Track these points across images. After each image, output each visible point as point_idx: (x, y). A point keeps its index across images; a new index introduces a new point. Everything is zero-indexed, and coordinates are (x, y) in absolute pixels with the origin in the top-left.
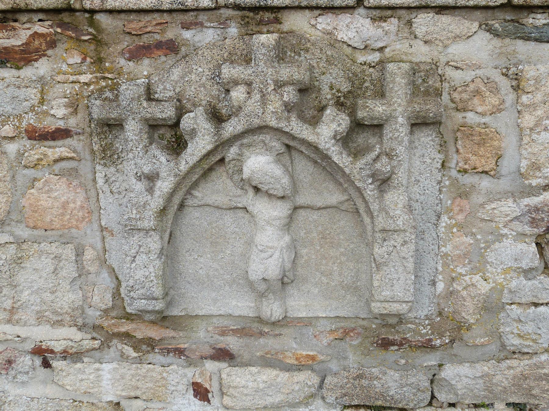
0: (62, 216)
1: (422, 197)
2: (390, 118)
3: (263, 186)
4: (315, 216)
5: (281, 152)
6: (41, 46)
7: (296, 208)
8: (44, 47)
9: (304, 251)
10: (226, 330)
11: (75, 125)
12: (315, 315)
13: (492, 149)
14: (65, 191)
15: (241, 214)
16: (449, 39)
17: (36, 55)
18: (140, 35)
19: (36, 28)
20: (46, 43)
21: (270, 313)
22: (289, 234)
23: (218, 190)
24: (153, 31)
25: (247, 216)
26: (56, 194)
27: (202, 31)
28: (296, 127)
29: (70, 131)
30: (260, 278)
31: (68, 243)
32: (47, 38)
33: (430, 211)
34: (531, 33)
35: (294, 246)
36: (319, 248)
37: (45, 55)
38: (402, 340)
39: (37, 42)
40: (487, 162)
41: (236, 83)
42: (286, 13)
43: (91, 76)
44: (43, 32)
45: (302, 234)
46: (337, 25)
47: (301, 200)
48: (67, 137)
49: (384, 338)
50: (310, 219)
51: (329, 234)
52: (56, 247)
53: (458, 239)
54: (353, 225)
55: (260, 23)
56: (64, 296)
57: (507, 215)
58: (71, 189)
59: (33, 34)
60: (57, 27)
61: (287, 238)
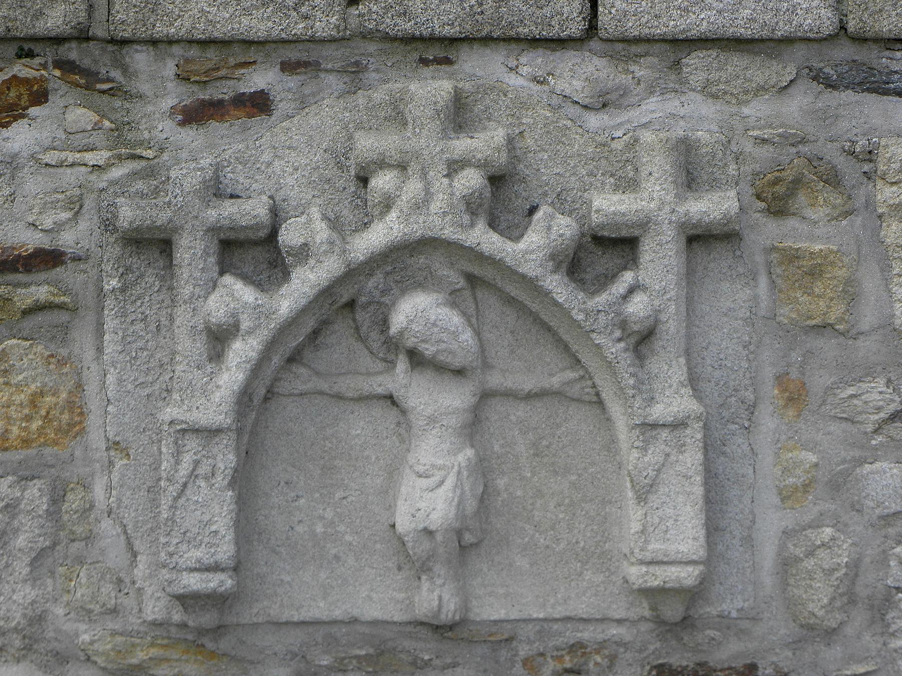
0: (27, 421)
1: (717, 374)
2: (645, 224)
3: (427, 346)
4: (520, 411)
5: (458, 286)
6: (20, 100)
7: (486, 395)
8: (24, 102)
9: (501, 483)
10: (344, 658)
11: (73, 244)
12: (524, 615)
13: (835, 282)
14: (40, 370)
15: (378, 410)
16: (746, 92)
17: (7, 116)
18: (205, 82)
19: (16, 69)
20: (30, 95)
21: (437, 603)
22: (472, 446)
23: (346, 360)
24: (229, 76)
25: (394, 411)
26: (20, 377)
27: (317, 77)
28: (483, 238)
29: (63, 254)
30: (419, 529)
31: (33, 478)
32: (32, 86)
33: (733, 399)
34: (888, 83)
35: (483, 469)
36: (529, 475)
37: (23, 116)
38: (698, 668)
39: (13, 94)
40: (831, 307)
41: (382, 164)
42: (465, 49)
43: (110, 154)
44: (28, 76)
45: (496, 448)
46: (555, 67)
47: (495, 380)
48: (55, 266)
49: (662, 665)
50: (512, 418)
51: (548, 447)
52: (10, 487)
53: (790, 455)
54: (591, 428)
55: (424, 62)
56: (14, 591)
57: (879, 409)
58: (52, 367)
59: (10, 79)
60: (54, 68)
61: (470, 452)
